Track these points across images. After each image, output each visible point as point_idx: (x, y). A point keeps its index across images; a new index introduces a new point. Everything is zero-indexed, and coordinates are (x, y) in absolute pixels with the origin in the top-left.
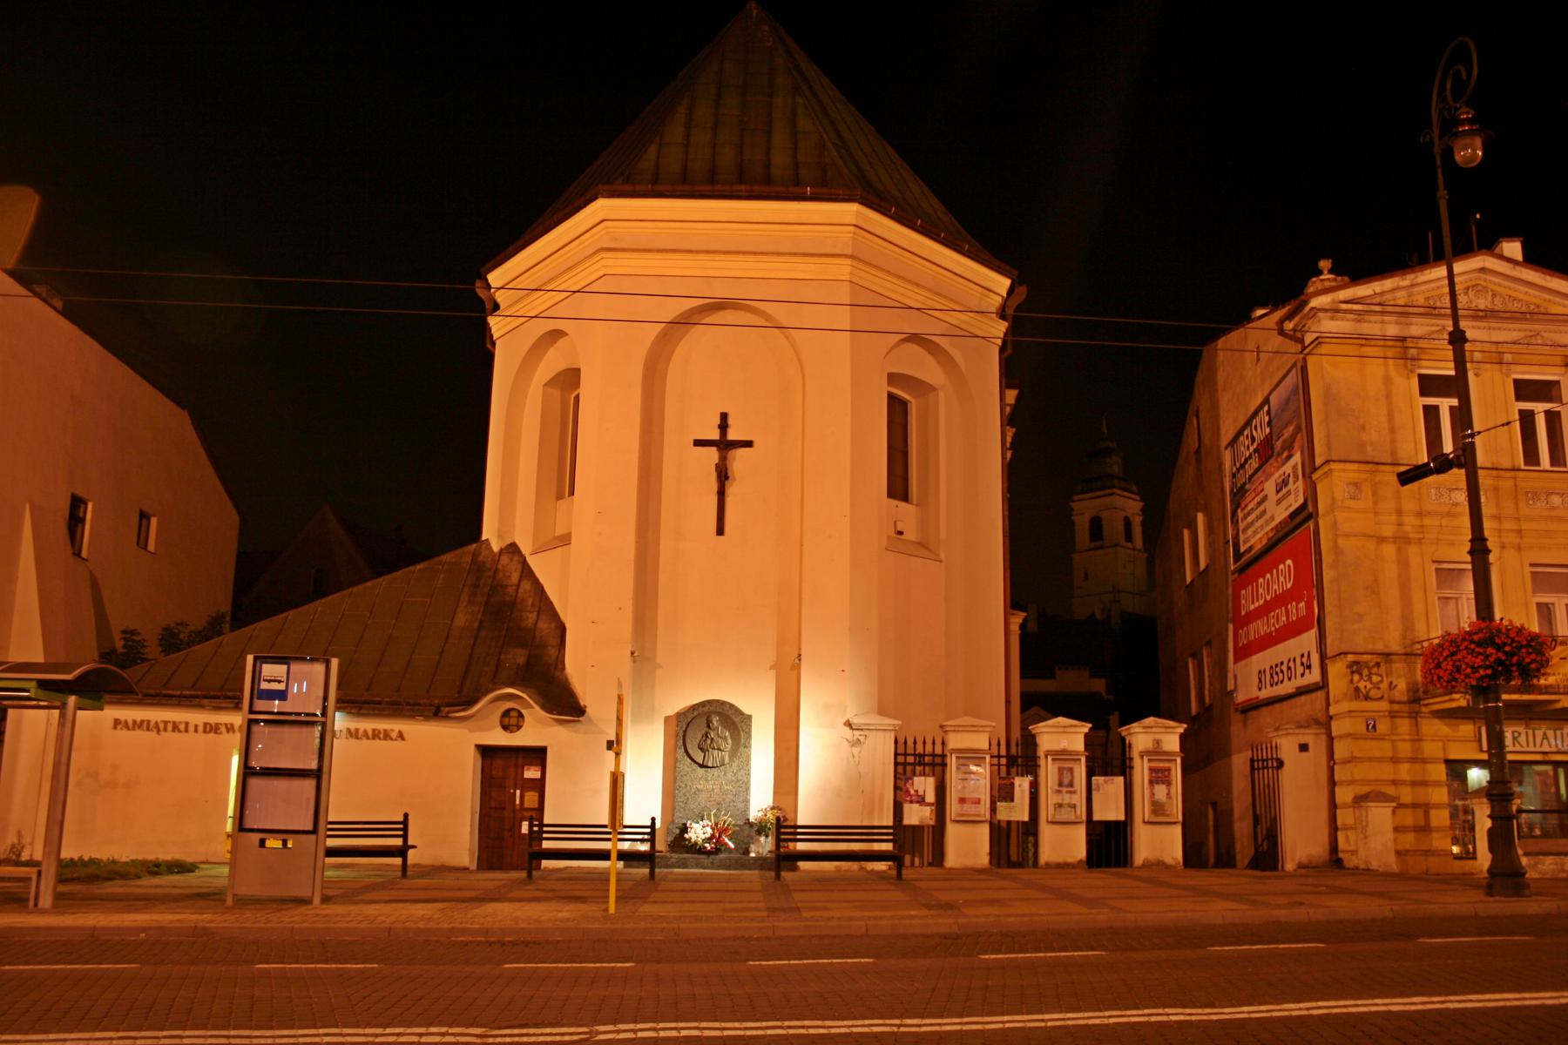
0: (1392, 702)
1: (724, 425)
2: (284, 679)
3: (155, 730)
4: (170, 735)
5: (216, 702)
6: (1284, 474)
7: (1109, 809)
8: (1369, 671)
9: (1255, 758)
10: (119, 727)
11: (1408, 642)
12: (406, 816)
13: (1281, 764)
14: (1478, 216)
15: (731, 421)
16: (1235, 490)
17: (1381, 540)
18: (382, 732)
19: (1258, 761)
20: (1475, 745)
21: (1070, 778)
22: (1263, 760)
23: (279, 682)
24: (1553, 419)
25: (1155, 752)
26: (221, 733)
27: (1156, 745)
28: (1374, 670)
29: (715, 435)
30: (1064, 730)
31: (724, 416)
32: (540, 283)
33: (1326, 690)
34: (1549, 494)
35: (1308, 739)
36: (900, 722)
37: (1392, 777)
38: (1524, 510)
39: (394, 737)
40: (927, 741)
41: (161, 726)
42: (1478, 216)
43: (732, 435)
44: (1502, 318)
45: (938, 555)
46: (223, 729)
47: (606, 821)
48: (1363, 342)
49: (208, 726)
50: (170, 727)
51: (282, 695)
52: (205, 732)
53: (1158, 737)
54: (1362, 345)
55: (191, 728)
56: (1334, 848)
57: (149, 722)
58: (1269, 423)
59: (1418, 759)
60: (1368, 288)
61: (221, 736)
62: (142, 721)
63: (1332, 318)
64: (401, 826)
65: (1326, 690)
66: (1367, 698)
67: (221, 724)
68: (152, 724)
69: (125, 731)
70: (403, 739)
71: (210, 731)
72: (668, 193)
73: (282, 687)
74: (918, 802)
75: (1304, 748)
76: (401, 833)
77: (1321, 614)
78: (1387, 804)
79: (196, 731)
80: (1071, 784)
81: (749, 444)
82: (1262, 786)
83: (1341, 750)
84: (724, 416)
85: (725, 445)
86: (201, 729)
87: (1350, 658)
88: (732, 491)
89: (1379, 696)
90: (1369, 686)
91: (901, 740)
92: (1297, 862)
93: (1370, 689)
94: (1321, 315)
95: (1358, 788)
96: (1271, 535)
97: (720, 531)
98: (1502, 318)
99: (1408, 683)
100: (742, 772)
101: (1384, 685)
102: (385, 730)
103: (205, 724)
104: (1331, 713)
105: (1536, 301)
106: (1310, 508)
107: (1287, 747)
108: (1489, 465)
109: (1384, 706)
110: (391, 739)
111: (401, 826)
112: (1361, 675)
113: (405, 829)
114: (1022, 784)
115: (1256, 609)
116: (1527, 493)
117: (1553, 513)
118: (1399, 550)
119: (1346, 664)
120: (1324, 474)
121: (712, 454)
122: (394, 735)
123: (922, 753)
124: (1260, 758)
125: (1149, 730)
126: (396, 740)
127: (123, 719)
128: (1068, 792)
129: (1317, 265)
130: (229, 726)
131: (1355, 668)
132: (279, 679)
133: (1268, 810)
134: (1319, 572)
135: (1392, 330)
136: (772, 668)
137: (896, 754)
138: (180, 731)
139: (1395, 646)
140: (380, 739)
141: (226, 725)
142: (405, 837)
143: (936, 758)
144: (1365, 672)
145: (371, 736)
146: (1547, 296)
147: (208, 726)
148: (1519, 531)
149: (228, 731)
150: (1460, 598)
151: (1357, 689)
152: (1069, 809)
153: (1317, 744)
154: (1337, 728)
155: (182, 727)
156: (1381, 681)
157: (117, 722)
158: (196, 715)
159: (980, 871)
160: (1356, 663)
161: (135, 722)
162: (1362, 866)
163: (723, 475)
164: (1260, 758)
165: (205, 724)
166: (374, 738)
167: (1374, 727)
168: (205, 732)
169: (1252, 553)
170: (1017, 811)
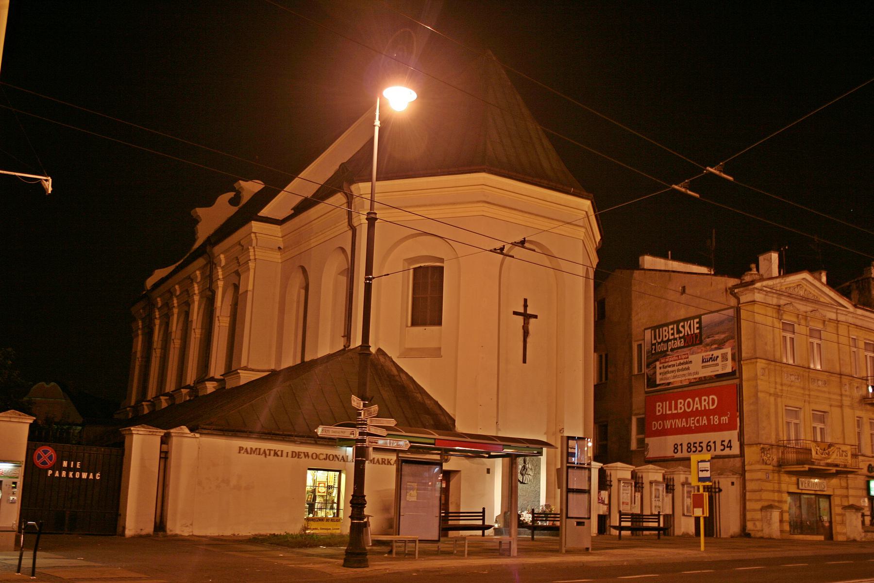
3: (264, 455)
4: (272, 458)
5: (303, 440)
10: (242, 452)
11: (777, 441)
12: (484, 509)
14: (787, 247)
17: (770, 394)
20: (796, 486)
24: (792, 339)
26: (301, 458)
30: (622, 469)
34: (818, 380)
35: (734, 480)
38: (811, 386)
41: (268, 452)
42: (787, 247)
43: (530, 311)
44: (822, 305)
46: (302, 455)
47: (559, 512)
48: (768, 305)
49: (294, 453)
50: (272, 453)
53: (687, 476)
54: (767, 307)
55: (285, 454)
56: (744, 527)
57: (260, 449)
59: (780, 491)
61: (301, 459)
62: (256, 449)
63: (759, 293)
64: (481, 514)
66: (766, 464)
67: (301, 452)
68: (262, 451)
69: (245, 454)
72: (514, 177)
74: (602, 503)
75: (733, 484)
76: (481, 518)
79: (287, 456)
83: (750, 486)
84: (525, 300)
85: (527, 317)
86: (290, 455)
87: (762, 446)
88: (529, 340)
94: (755, 290)
95: (763, 503)
97: (524, 361)
98: (822, 305)
100: (537, 486)
103: (251, 448)
105: (816, 295)
108: (801, 365)
110: (391, 464)
111: (481, 514)
112: (764, 454)
113: (484, 516)
116: (812, 379)
117: (819, 388)
118: (775, 399)
119: (760, 448)
120: (751, 362)
121: (520, 319)
127: (245, 447)
129: (750, 266)
130: (306, 454)
135: (775, 301)
136: (545, 434)
138: (278, 456)
139: (774, 443)
140: (385, 464)
141: (304, 453)
142: (483, 520)
144: (765, 453)
145: (381, 462)
146: (820, 293)
147: (294, 453)
148: (809, 395)
149: (305, 457)
150: (791, 422)
155: (279, 453)
156: (770, 457)
157: (241, 449)
158: (267, 444)
159: (148, 536)
160: (763, 448)
161: (251, 448)
162: (766, 536)
165: (293, 452)
166: (382, 464)
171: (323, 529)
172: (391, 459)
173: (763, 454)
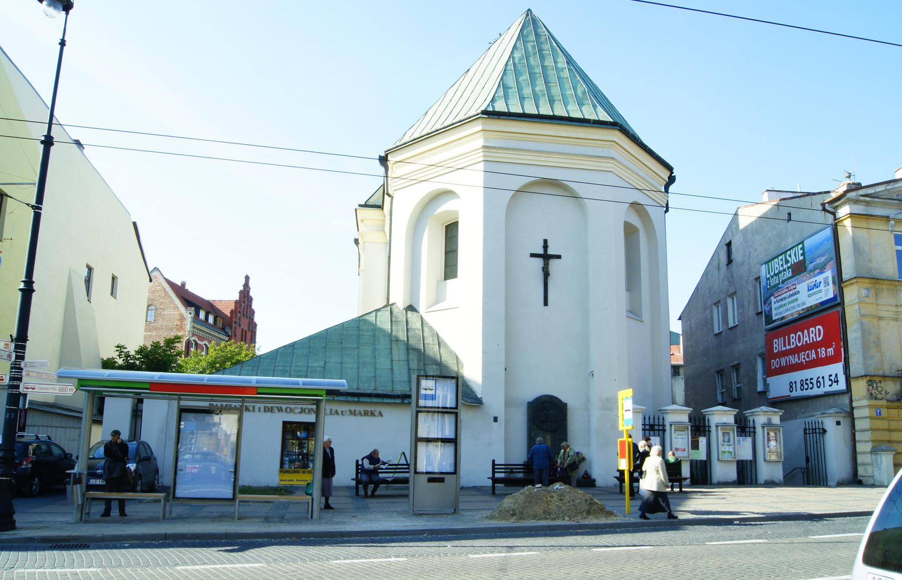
0: (888, 401)
1: (545, 246)
2: (434, 388)
6: (816, 281)
7: (745, 453)
8: (876, 385)
9: (807, 428)
13: (825, 431)
15: (549, 244)
16: (768, 287)
18: (370, 411)
19: (809, 429)
21: (728, 438)
22: (813, 429)
23: (431, 390)
25: (769, 424)
27: (769, 421)
28: (879, 385)
29: (541, 252)
31: (545, 241)
32: (435, 163)
33: (850, 394)
35: (841, 419)
36: (645, 408)
37: (888, 439)
39: (377, 415)
40: (696, 419)
43: (550, 252)
45: (641, 318)
51: (433, 397)
52: (265, 411)
58: (803, 254)
60: (873, 189)
64: (496, 470)
65: (850, 394)
66: (876, 398)
70: (381, 415)
71: (268, 411)
73: (433, 392)
75: (838, 423)
77: (847, 356)
78: (891, 453)
80: (729, 441)
81: (559, 257)
82: (812, 442)
84: (545, 241)
89: (882, 397)
90: (877, 392)
91: (647, 418)
92: (837, 482)
93: (877, 394)
96: (801, 312)
97: (546, 304)
99: (181, 336)
101: (883, 392)
102: (371, 411)
104: (853, 406)
106: (839, 300)
107: (829, 424)
109: (884, 403)
111: (496, 470)
112: (873, 387)
114: (702, 441)
115: (786, 350)
121: (539, 262)
122: (376, 413)
123: (653, 423)
124: (811, 428)
125: (766, 413)
126: (378, 416)
128: (728, 445)
131: (870, 383)
132: (431, 388)
133: (816, 454)
134: (845, 333)
137: (644, 425)
138: (249, 411)
140: (368, 415)
143: (646, 426)
144: (875, 386)
149: (279, 411)
151: (871, 394)
152: (728, 454)
153: (845, 423)
154: (856, 413)
156: (882, 390)
160: (870, 381)
163: (546, 274)
164: (811, 428)
166: (365, 415)
167: (880, 413)
168: (265, 411)
169: (783, 321)
170: (701, 455)
171: (300, 480)
172: (375, 411)
173: (871, 387)
